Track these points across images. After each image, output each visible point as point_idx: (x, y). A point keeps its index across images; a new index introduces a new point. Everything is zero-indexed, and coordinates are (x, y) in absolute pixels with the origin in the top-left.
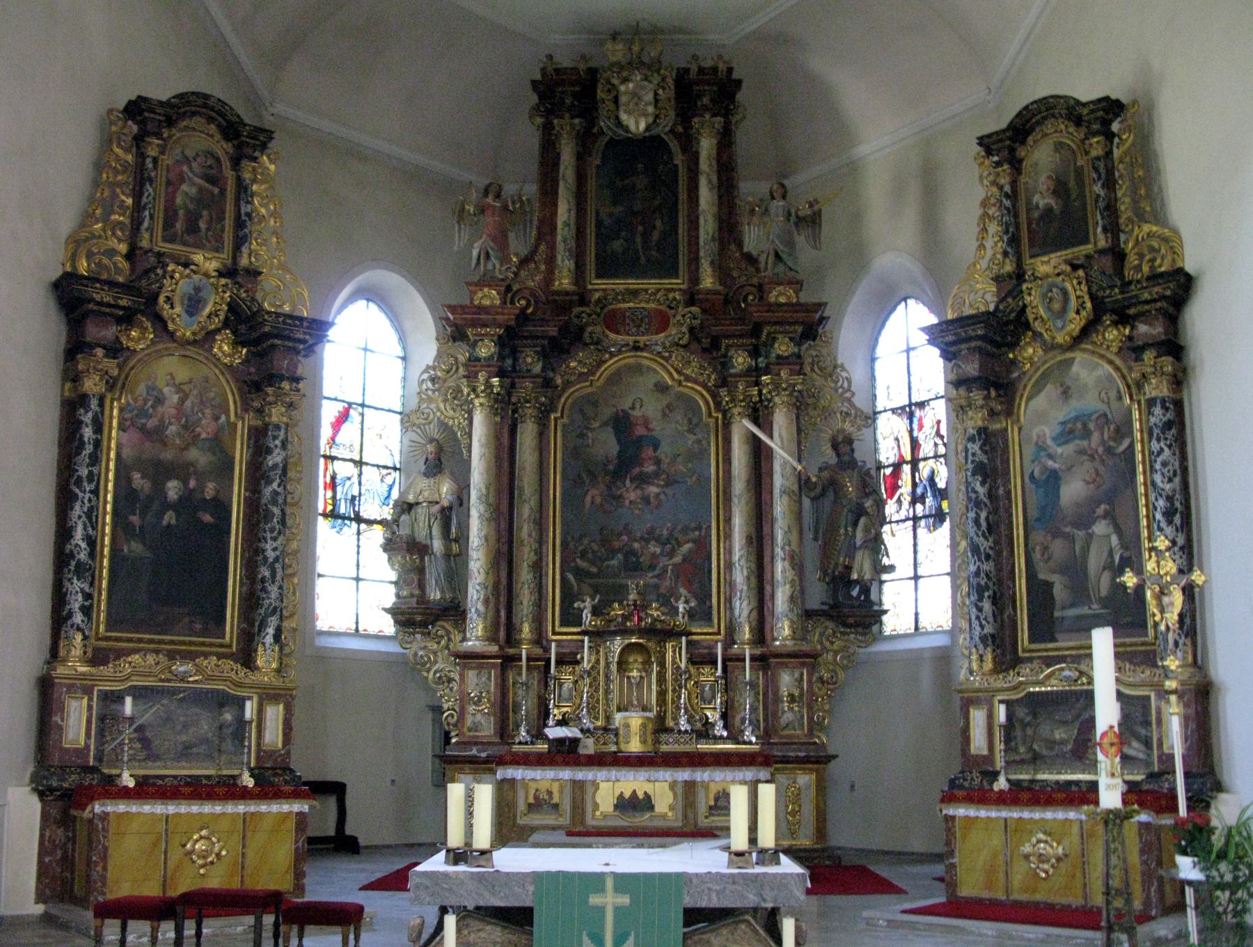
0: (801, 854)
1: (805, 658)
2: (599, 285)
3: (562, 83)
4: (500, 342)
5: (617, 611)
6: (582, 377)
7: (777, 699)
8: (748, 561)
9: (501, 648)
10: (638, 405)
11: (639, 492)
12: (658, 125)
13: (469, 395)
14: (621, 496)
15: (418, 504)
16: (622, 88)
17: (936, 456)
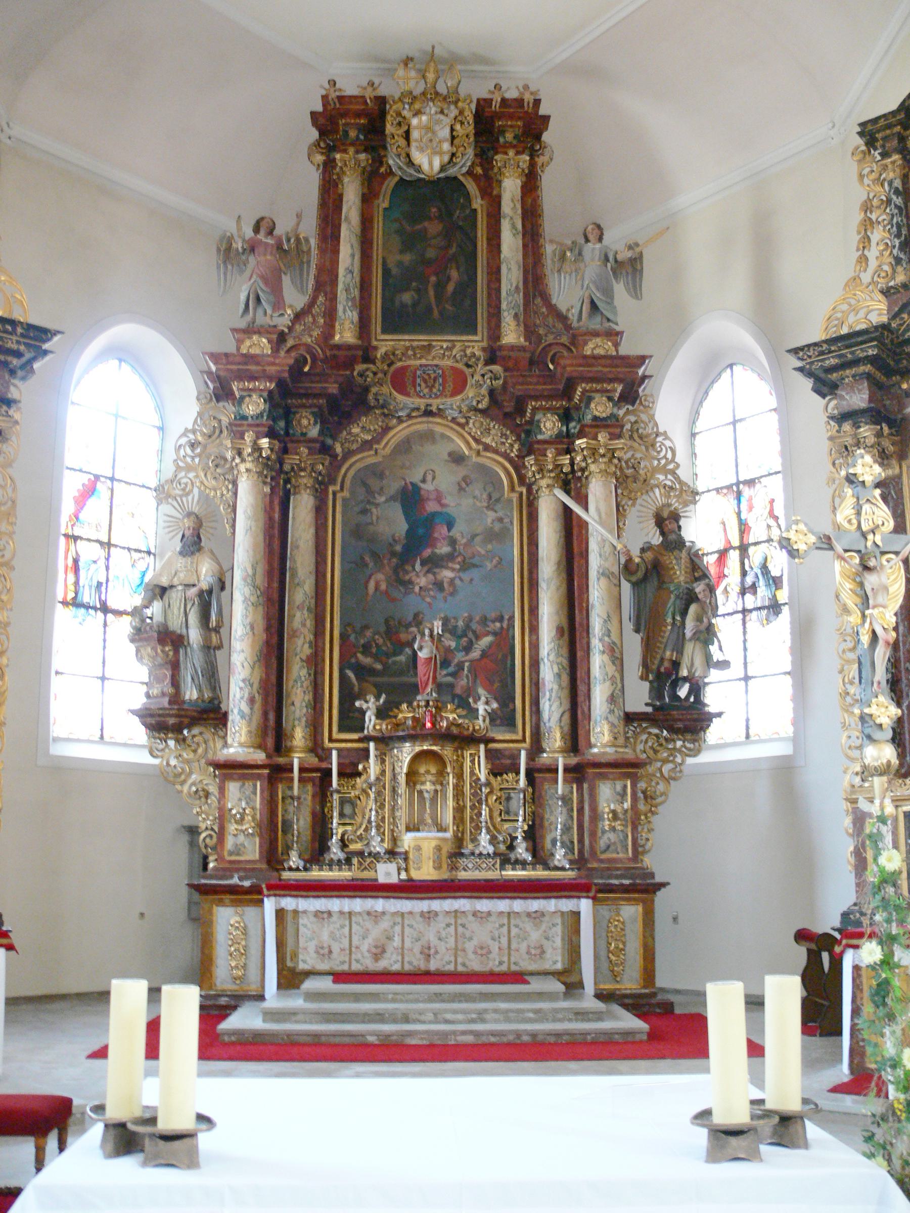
0: (627, 1001)
1: (627, 768)
2: (385, 343)
3: (344, 115)
4: (270, 398)
5: (405, 713)
6: (367, 445)
7: (596, 816)
8: (558, 655)
9: (269, 756)
10: (429, 478)
11: (430, 576)
12: (455, 164)
13: (233, 459)
14: (410, 582)
15: (172, 587)
16: (415, 122)
17: (770, 540)
